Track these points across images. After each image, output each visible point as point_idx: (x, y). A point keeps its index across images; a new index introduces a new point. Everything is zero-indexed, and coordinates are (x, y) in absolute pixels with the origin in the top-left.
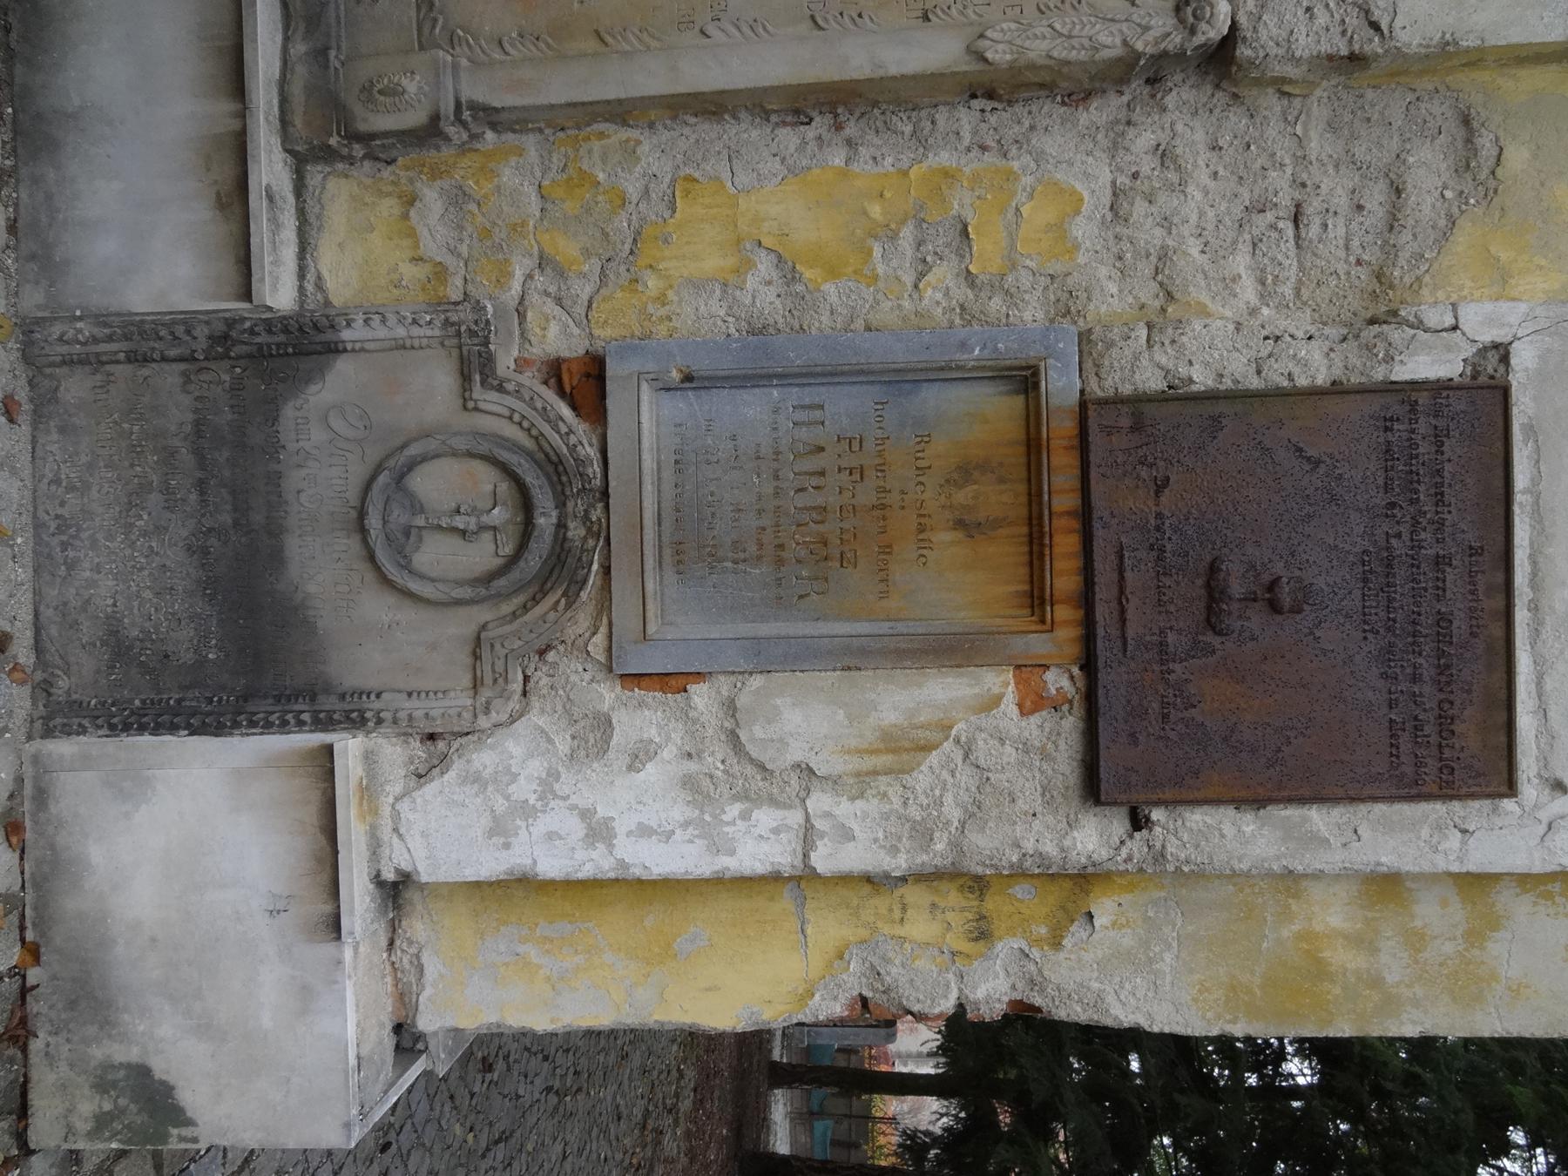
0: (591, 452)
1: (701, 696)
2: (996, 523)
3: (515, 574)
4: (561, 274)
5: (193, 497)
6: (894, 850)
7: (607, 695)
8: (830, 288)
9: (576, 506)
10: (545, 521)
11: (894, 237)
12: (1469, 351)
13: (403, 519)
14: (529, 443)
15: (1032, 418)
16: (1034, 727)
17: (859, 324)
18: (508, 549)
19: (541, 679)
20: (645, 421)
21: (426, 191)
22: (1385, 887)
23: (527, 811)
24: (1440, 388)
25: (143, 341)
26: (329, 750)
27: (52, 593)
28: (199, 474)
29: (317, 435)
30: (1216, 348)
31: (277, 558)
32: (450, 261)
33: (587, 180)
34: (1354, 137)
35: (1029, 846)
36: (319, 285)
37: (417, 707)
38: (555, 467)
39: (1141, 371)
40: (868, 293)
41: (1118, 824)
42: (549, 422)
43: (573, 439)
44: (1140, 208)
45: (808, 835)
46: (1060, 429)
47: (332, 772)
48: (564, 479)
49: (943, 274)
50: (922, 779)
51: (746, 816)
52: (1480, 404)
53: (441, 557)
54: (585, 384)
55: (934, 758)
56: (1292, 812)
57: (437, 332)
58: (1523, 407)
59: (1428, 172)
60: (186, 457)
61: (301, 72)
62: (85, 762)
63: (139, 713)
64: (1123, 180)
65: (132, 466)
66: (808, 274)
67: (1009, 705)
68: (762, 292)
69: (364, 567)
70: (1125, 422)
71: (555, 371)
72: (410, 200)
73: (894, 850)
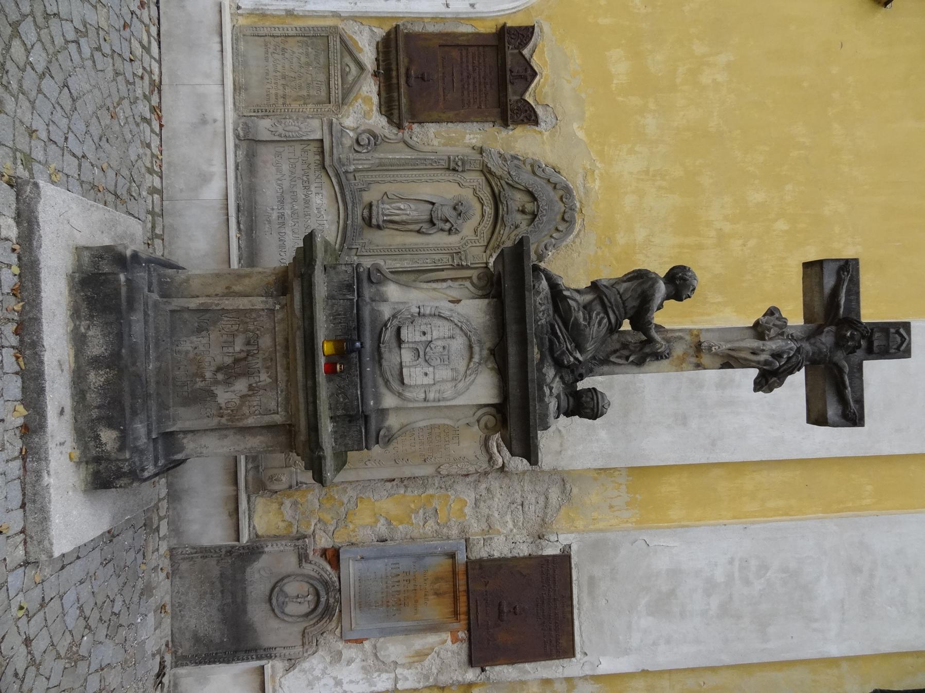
0: (336, 579)
1: (367, 645)
2: (445, 593)
3: (315, 614)
4: (325, 524)
5: (220, 595)
6: (419, 682)
7: (341, 645)
8: (400, 527)
9: (332, 594)
10: (323, 600)
11: (418, 512)
12: (561, 547)
14: (318, 577)
15: (454, 565)
16: (455, 647)
17: (408, 537)
18: (312, 607)
19: (322, 641)
20: (351, 569)
22: (547, 682)
23: (318, 679)
24: (554, 556)
25: (205, 552)
26: (263, 667)
29: (257, 576)
30: (499, 548)
31: (245, 611)
33: (332, 498)
34: (536, 484)
35: (455, 678)
36: (254, 528)
37: (286, 652)
38: (326, 584)
39: (481, 552)
40: (411, 528)
41: (478, 670)
44: (482, 504)
45: (396, 680)
46: (461, 569)
47: (263, 673)
49: (431, 523)
50: (426, 663)
51: (379, 676)
52: (563, 560)
53: (293, 608)
54: (333, 557)
55: (430, 657)
56: (521, 665)
58: (574, 561)
59: (554, 494)
60: (218, 584)
61: (251, 473)
62: (189, 675)
63: (204, 658)
64: (478, 497)
66: (395, 523)
67: (449, 642)
68: (382, 528)
70: (477, 567)
71: (324, 553)
72: (282, 504)
73: (419, 682)
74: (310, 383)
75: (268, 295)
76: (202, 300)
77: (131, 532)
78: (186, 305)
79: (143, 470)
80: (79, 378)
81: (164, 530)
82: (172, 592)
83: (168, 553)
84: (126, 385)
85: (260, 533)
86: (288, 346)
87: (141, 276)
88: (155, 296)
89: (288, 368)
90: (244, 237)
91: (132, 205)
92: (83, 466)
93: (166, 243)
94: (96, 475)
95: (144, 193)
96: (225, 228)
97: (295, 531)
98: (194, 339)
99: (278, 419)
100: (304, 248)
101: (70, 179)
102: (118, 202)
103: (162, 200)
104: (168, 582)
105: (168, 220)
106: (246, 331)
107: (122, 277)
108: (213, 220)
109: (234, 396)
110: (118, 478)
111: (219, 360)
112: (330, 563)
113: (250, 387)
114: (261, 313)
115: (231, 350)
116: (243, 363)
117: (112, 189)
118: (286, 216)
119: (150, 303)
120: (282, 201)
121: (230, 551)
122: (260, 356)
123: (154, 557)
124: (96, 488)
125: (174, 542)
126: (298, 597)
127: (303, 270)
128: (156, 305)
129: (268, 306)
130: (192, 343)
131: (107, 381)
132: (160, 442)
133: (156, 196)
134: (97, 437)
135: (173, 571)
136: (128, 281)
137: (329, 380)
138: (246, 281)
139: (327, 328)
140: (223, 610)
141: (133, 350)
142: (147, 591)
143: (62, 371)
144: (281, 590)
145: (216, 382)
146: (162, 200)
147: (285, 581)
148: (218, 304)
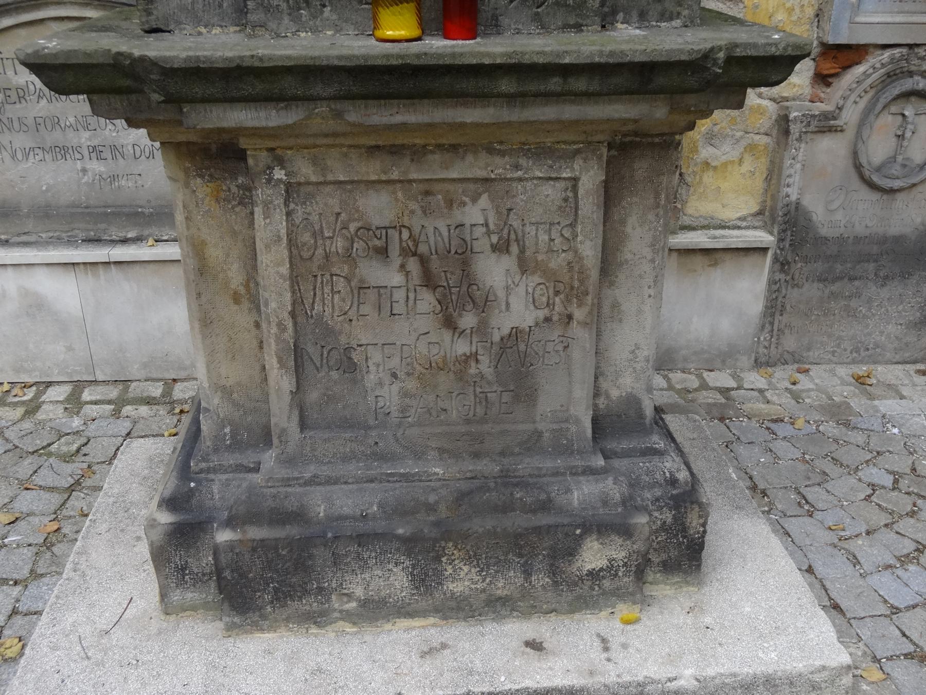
0: (887, 54)
5: (857, 283)
13: (898, 168)
21: (702, 156)
25: (774, 307)
27: (888, 355)
28: (846, 280)
29: (839, 216)
31: (899, 239)
32: (744, 143)
38: (891, 77)
42: (864, 80)
43: (878, 65)
48: (898, 71)
57: (803, 145)
60: (835, 287)
65: (834, 315)
69: (915, 191)
72: (707, 164)
74: (506, 85)
75: (246, 199)
76: (272, 362)
77: (741, 450)
78: (287, 398)
79: (673, 482)
80: (459, 609)
81: (721, 379)
82: (830, 362)
83: (762, 371)
84: (480, 525)
85: (755, 208)
86: (390, 148)
87: (220, 491)
88: (269, 459)
89: (454, 148)
90: (155, 231)
91: (96, 452)
92: (649, 590)
93: (182, 374)
94: (668, 567)
95: (76, 423)
96: (137, 268)
97: (765, 140)
98: (371, 379)
99: (590, 177)
100: (90, 91)
101: (22, 607)
102: (88, 482)
103: (95, 382)
104: (815, 371)
105: (135, 371)
106: (348, 256)
107: (224, 536)
108: (121, 292)
109: (521, 290)
110: (684, 529)
111: (424, 323)
112: (846, 67)
113: (502, 248)
114: (298, 217)
115: (400, 295)
116: (435, 265)
117: (56, 499)
118: (95, 142)
119: (284, 473)
120: (62, 151)
121: (782, 264)
122: (416, 223)
123: (775, 399)
124: (699, 567)
125: (745, 361)
126: (900, 137)
127: (156, 97)
128: (289, 461)
129: (280, 201)
130: (381, 384)
131: (471, 558)
132: (611, 445)
133: (86, 396)
134: (594, 575)
135: (795, 362)
136: (230, 523)
137: (495, 27)
138: (214, 253)
139: (338, 30)
140: (886, 278)
141: (402, 511)
142: (839, 413)
143: (444, 646)
144: (878, 169)
145: (482, 329)
146: (95, 382)
147: (863, 161)
148: (281, 327)
